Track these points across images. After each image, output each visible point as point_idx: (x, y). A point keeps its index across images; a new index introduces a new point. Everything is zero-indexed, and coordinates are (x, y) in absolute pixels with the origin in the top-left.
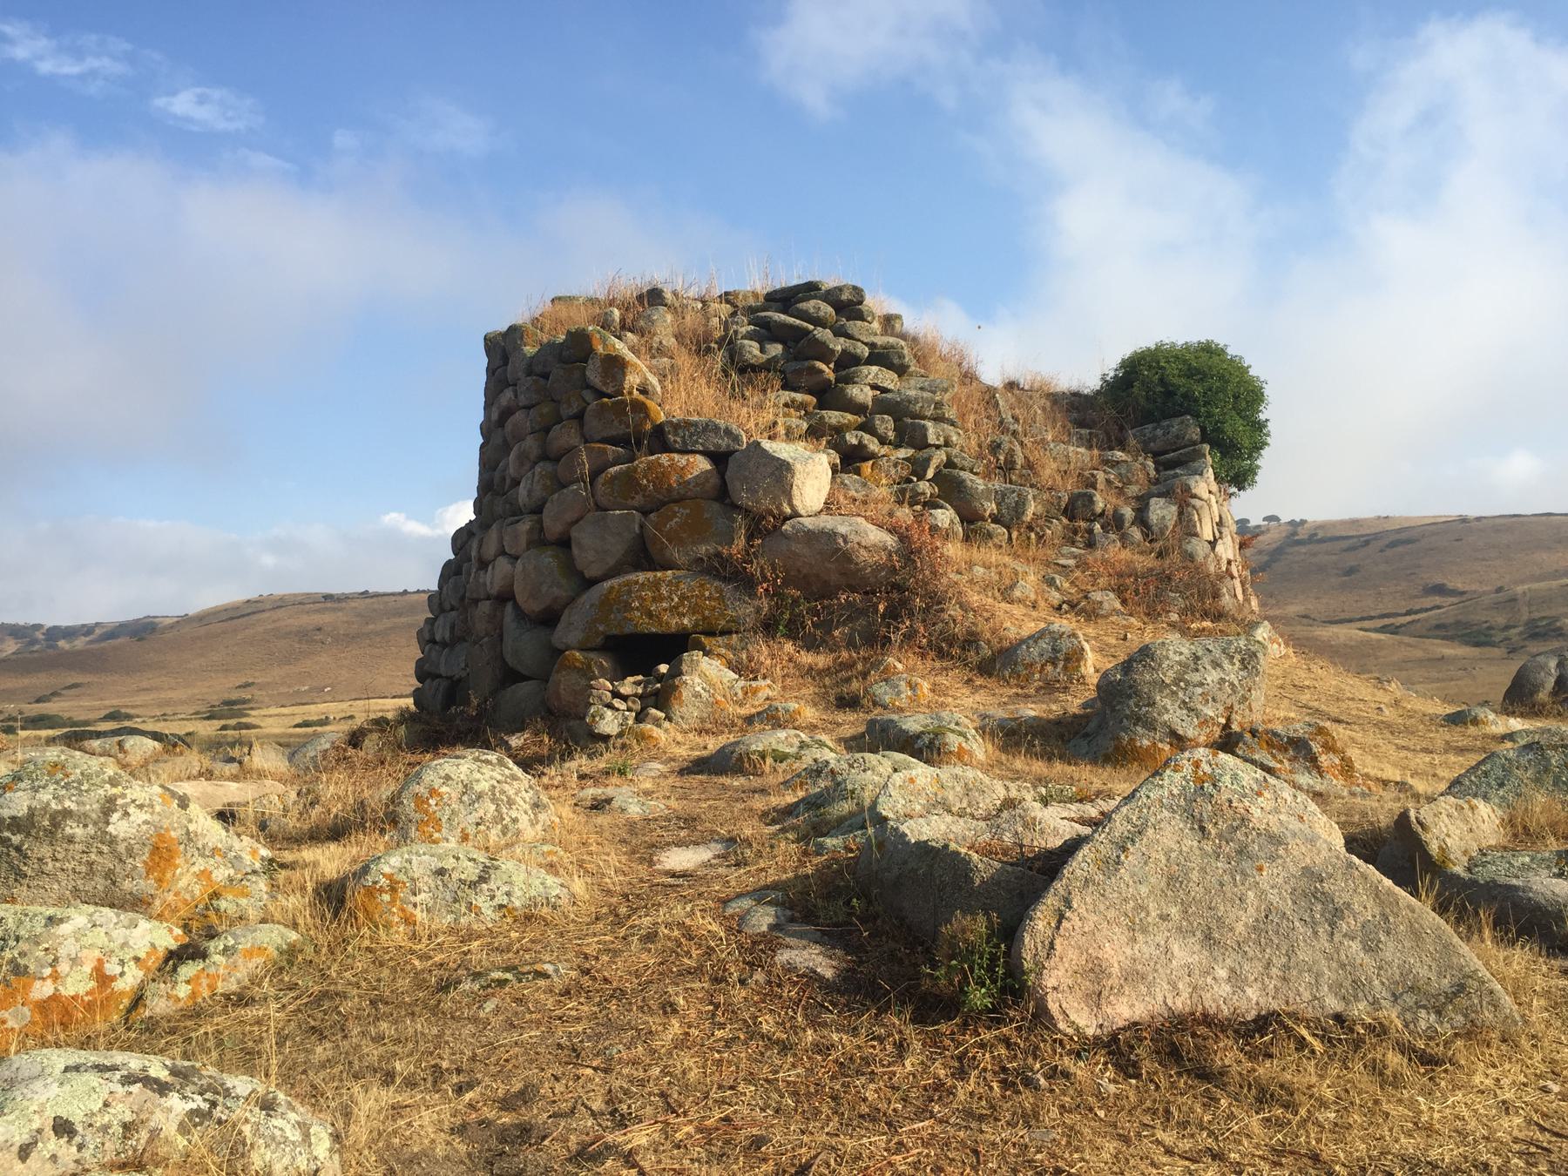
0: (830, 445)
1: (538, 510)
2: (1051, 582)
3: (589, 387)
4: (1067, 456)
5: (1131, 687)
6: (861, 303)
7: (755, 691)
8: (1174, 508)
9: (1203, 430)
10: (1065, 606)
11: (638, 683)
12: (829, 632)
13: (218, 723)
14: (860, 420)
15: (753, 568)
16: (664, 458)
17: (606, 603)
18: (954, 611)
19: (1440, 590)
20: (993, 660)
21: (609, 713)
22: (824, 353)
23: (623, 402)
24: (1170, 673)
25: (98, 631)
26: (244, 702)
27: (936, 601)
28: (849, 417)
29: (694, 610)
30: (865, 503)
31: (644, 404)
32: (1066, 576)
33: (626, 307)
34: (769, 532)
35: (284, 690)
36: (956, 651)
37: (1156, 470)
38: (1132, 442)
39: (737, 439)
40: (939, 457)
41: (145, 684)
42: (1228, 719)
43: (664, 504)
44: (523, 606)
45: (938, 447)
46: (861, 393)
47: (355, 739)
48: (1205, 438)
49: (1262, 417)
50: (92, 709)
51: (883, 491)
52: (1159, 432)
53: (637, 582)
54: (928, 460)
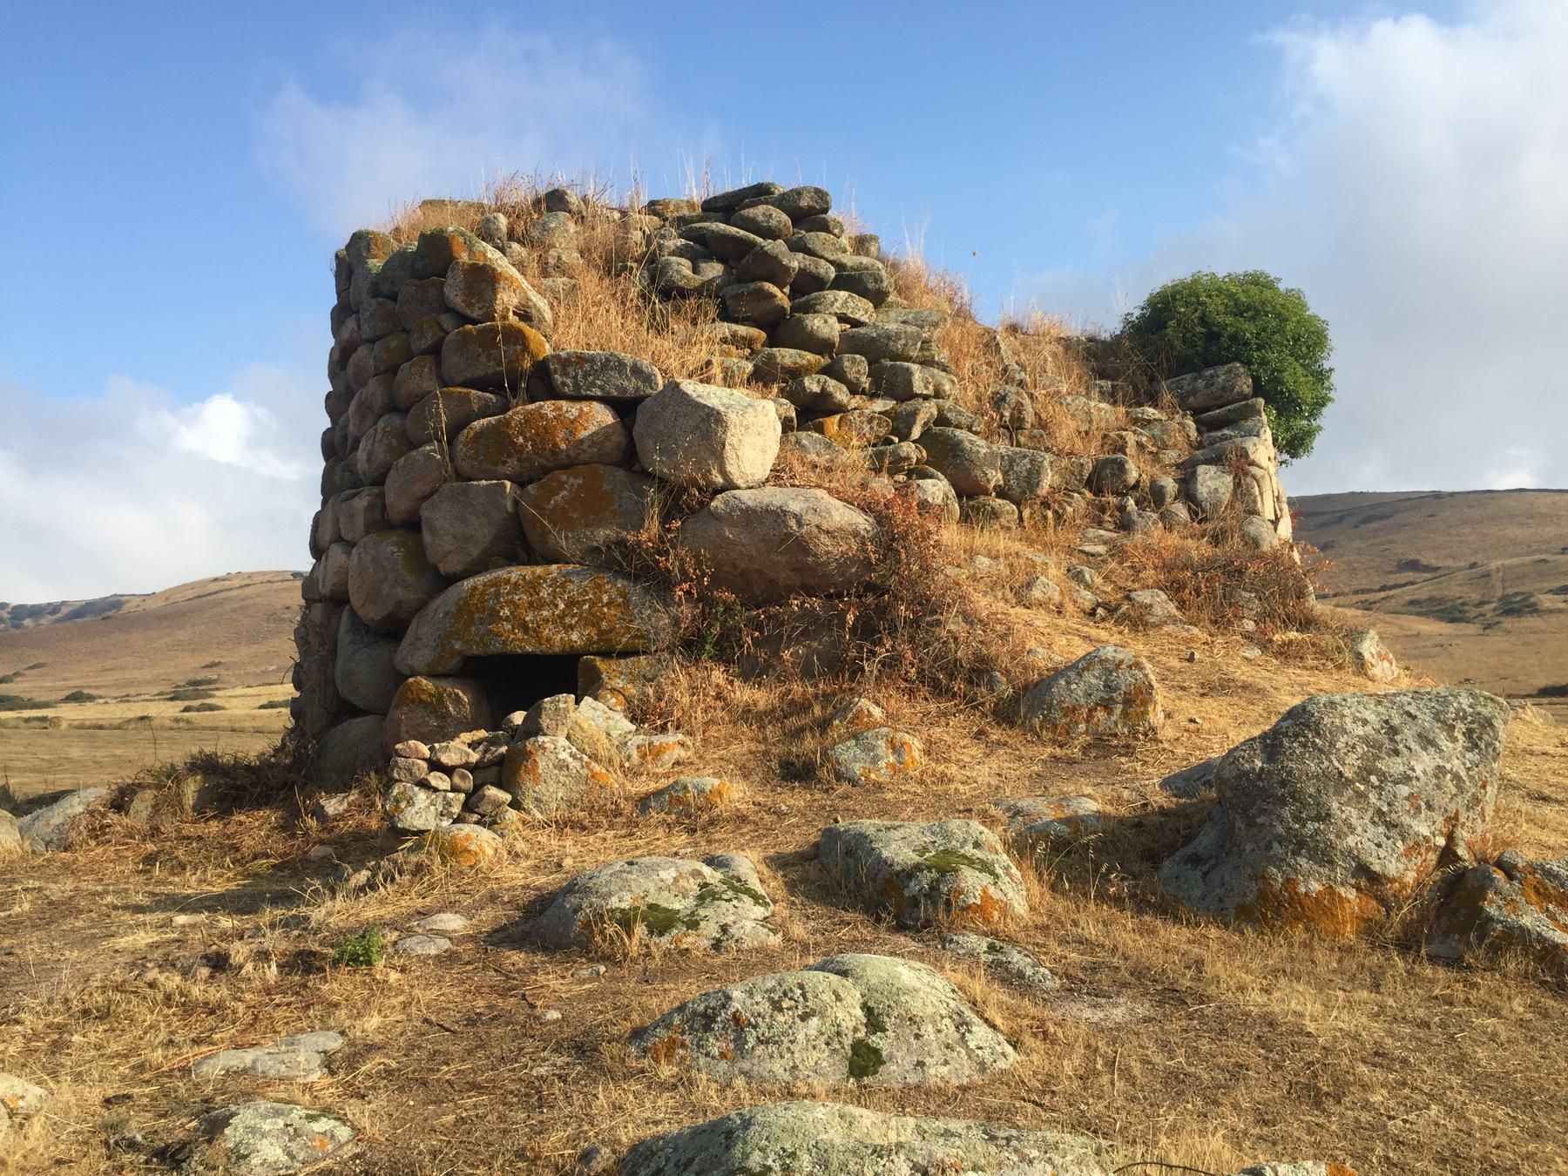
0: (783, 393)
1: (380, 481)
2: (1078, 577)
3: (450, 310)
4: (1088, 413)
5: (1283, 784)
6: (825, 211)
7: (657, 753)
8: (1229, 479)
9: (1256, 380)
10: (1100, 611)
11: (473, 745)
12: (776, 654)
13: (181, 704)
14: (824, 361)
15: (671, 563)
16: (548, 407)
17: (464, 610)
18: (955, 625)
19: (1414, 565)
20: (1015, 700)
21: (422, 796)
22: (776, 272)
23: (494, 330)
24: (1352, 759)
25: (65, 610)
26: (210, 682)
27: (928, 607)
28: (810, 356)
29: (592, 620)
30: (829, 470)
31: (520, 331)
32: (1098, 568)
33: (514, 213)
34: (693, 511)
35: (251, 669)
36: (959, 686)
37: (1198, 430)
38: (1167, 397)
39: (648, 379)
40: (928, 411)
41: (109, 663)
42: (1450, 837)
43: (547, 471)
44: (360, 612)
45: (926, 398)
46: (825, 325)
47: (120, 802)
48: (1258, 390)
49: (1326, 366)
50: (53, 689)
51: (854, 455)
52: (1200, 383)
53: (508, 581)
54: (913, 414)
